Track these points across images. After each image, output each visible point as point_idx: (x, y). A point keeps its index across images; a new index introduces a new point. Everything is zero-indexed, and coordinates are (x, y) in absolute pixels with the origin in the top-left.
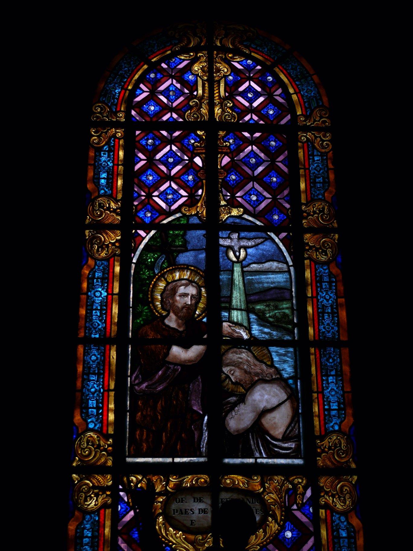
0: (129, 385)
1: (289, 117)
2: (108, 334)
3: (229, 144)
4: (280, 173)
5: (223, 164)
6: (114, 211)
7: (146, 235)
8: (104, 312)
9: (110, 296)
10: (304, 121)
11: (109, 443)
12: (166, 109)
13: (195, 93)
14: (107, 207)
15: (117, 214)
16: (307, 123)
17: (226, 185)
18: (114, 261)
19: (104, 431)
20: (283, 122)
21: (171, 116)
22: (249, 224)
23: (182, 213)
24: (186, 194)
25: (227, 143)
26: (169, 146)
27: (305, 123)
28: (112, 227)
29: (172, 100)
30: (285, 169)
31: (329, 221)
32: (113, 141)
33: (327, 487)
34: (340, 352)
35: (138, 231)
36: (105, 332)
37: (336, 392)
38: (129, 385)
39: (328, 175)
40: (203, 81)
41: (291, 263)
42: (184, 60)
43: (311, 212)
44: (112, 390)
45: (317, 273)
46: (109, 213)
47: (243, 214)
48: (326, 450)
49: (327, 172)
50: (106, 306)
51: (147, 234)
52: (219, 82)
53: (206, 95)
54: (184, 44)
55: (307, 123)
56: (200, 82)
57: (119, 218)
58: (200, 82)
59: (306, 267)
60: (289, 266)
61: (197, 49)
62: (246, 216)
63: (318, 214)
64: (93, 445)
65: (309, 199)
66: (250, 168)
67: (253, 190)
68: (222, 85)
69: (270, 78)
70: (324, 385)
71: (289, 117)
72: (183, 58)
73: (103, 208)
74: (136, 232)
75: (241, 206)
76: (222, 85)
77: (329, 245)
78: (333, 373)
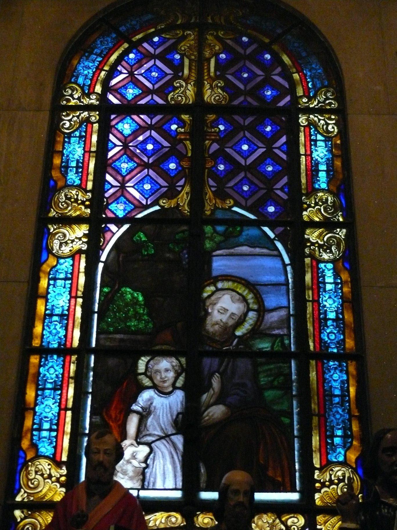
0: (83, 478)
1: (288, 98)
2: (68, 344)
3: (218, 130)
4: (276, 160)
5: (210, 153)
6: (83, 203)
7: (117, 229)
8: (80, 170)
9: (62, 412)
10: (306, 103)
11: (87, 197)
12: (146, 91)
13: (180, 74)
14: (74, 199)
15: (86, 207)
16: (309, 104)
17: (215, 174)
18: (89, 157)
19: (58, 459)
20: (281, 104)
21: (152, 99)
22: (237, 217)
23: (160, 206)
24: (166, 184)
25: (215, 129)
26: (151, 95)
27: (307, 105)
28: (79, 220)
29: (151, 139)
30: (284, 157)
31: (333, 213)
32: (86, 126)
33: (312, 211)
34: (347, 367)
35: (108, 225)
36: (66, 341)
37: (341, 414)
38: (83, 478)
39: (351, 425)
40: (191, 61)
41: (287, 260)
42: (169, 39)
43: (312, 203)
44: (69, 409)
45: (319, 273)
46: (77, 205)
47: (232, 207)
48: (313, 205)
49: (350, 420)
50: (82, 168)
51: (119, 228)
52: (208, 60)
53: (193, 74)
54: (170, 21)
55: (309, 104)
56: (186, 62)
57: (88, 211)
58: (186, 62)
59: (306, 266)
60: (285, 265)
61: (184, 27)
62: (235, 209)
63: (337, 485)
64: (42, 475)
65: (324, 463)
66: (242, 82)
67: (245, 82)
68: (213, 62)
69: (268, 56)
70: (327, 407)
71: (288, 98)
72: (167, 36)
73: (69, 199)
74: (106, 226)
75: (231, 197)
76: (213, 62)
77: (335, 243)
78: (337, 400)
